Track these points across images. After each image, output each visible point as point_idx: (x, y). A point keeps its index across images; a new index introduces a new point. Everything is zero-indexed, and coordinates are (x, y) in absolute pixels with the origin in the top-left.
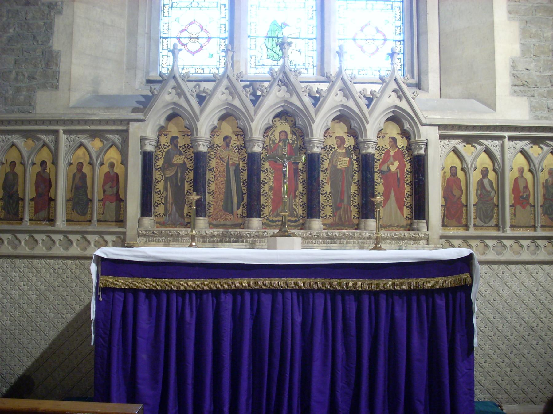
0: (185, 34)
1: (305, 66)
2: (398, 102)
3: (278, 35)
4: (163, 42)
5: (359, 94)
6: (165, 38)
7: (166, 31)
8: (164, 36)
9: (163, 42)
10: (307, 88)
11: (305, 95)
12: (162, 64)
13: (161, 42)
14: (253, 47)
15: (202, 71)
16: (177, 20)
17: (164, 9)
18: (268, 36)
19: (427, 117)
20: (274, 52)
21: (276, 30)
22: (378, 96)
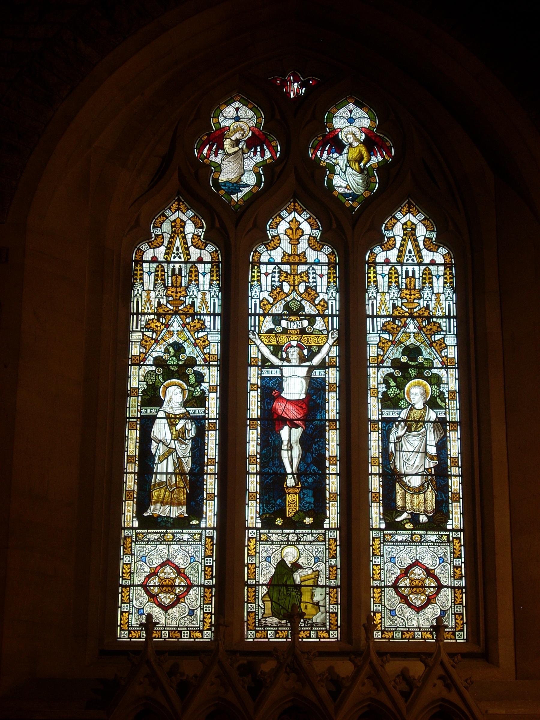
0: (155, 581)
1: (325, 626)
2: (445, 694)
3: (286, 581)
4: (122, 591)
5: (393, 683)
6: (126, 586)
7: (127, 576)
8: (124, 582)
9: (122, 591)
10: (325, 677)
11: (322, 686)
12: (121, 624)
13: (120, 591)
14: (251, 599)
15: (177, 635)
16: (143, 559)
17: (124, 543)
18: (272, 583)
19: (487, 712)
20: (281, 607)
21: (284, 575)
22: (419, 685)
